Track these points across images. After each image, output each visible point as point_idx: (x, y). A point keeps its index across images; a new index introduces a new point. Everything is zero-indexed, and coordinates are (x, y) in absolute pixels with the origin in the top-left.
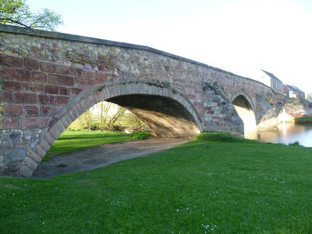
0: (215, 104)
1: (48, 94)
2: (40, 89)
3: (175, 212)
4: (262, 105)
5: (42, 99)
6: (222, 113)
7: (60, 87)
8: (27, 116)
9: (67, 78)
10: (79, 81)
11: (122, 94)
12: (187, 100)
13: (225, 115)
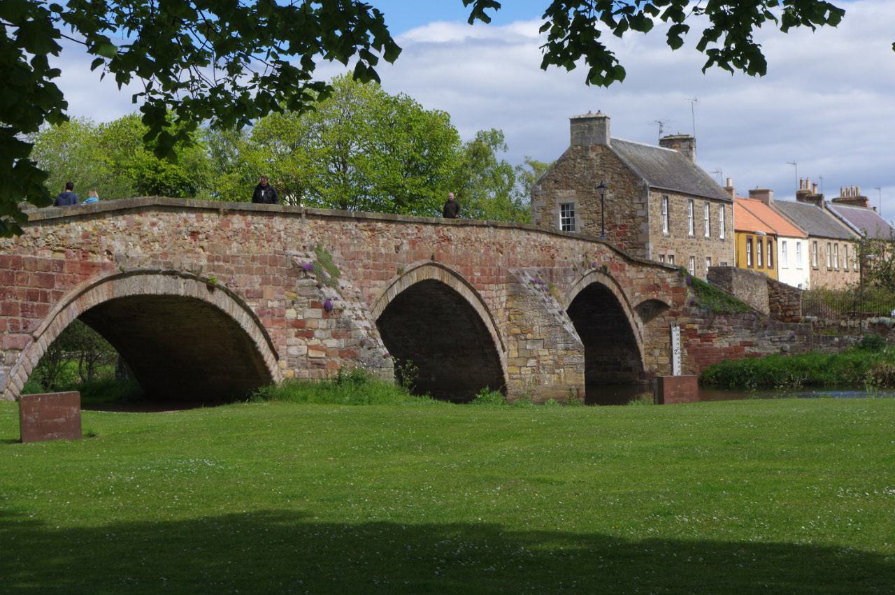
4: (529, 314)
6: (335, 336)
7: (41, 291)
8: (10, 333)
9: (48, 276)
10: (60, 281)
11: (115, 296)
12: (241, 304)
13: (342, 343)
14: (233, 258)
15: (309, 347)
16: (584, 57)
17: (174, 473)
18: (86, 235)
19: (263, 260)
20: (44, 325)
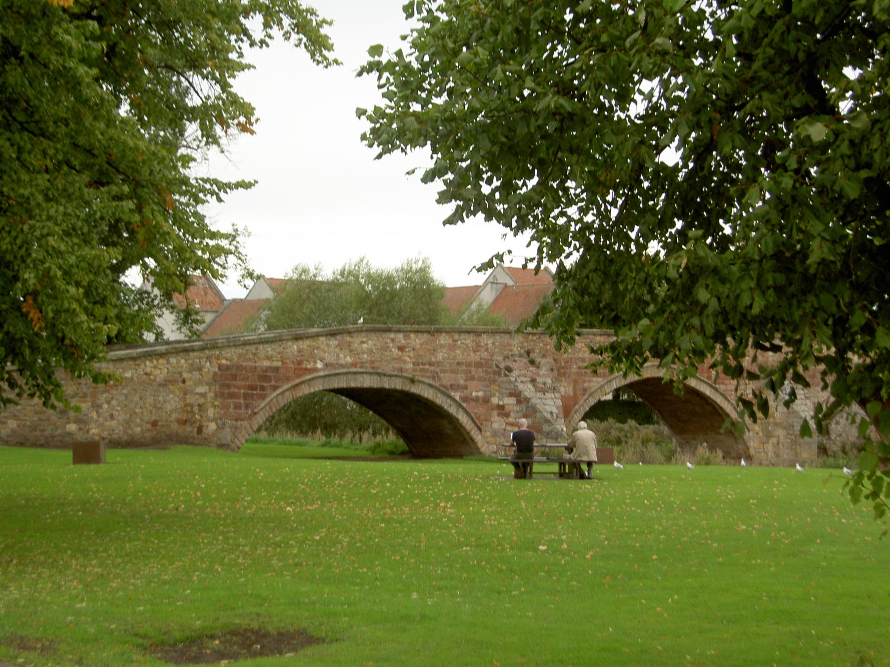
0: (512, 401)
1: (250, 392)
2: (244, 387)
3: (371, 562)
5: (246, 396)
6: (525, 416)
9: (266, 376)
14: (438, 364)
15: (507, 424)
16: (861, 72)
17: (377, 486)
18: (300, 351)
19: (468, 364)
20: (263, 405)
